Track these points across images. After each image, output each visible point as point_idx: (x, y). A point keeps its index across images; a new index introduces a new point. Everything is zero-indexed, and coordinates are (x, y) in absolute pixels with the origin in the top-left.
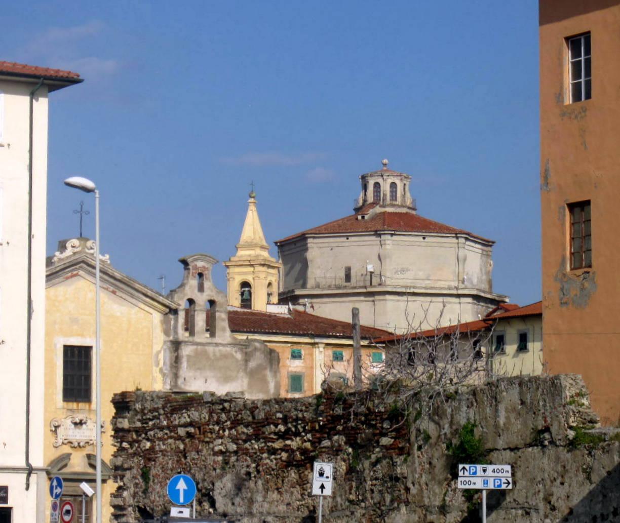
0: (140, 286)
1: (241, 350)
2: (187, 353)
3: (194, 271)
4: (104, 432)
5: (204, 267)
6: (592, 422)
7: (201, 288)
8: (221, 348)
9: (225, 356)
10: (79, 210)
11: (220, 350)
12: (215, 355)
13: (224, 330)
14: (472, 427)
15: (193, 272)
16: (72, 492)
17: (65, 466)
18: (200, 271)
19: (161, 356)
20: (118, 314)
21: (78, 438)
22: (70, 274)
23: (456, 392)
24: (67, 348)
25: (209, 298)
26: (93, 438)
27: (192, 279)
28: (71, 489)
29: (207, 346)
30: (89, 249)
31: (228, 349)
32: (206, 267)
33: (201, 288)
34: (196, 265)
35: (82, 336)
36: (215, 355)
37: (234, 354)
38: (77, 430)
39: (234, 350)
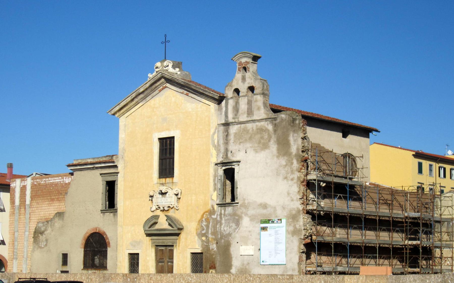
0: (158, 84)
1: (271, 122)
2: (234, 131)
3: (240, 67)
4: (180, 199)
5: (246, 62)
6: (290, 253)
7: (244, 79)
8: (257, 123)
9: (261, 130)
10: (164, 41)
11: (257, 126)
12: (253, 130)
13: (259, 109)
14: (226, 216)
15: (239, 68)
16: (161, 243)
17: (156, 223)
18: (244, 66)
19: (216, 137)
20: (190, 110)
21: (164, 204)
22: (162, 87)
23: (239, 140)
24: (160, 139)
25: (249, 85)
26: (173, 203)
27: (238, 73)
28: (161, 241)
29: (247, 123)
30: (165, 67)
31: (262, 123)
32: (248, 61)
33: (244, 79)
34: (241, 62)
35: (168, 130)
36: (253, 130)
37: (267, 126)
38: (163, 198)
39: (266, 123)
